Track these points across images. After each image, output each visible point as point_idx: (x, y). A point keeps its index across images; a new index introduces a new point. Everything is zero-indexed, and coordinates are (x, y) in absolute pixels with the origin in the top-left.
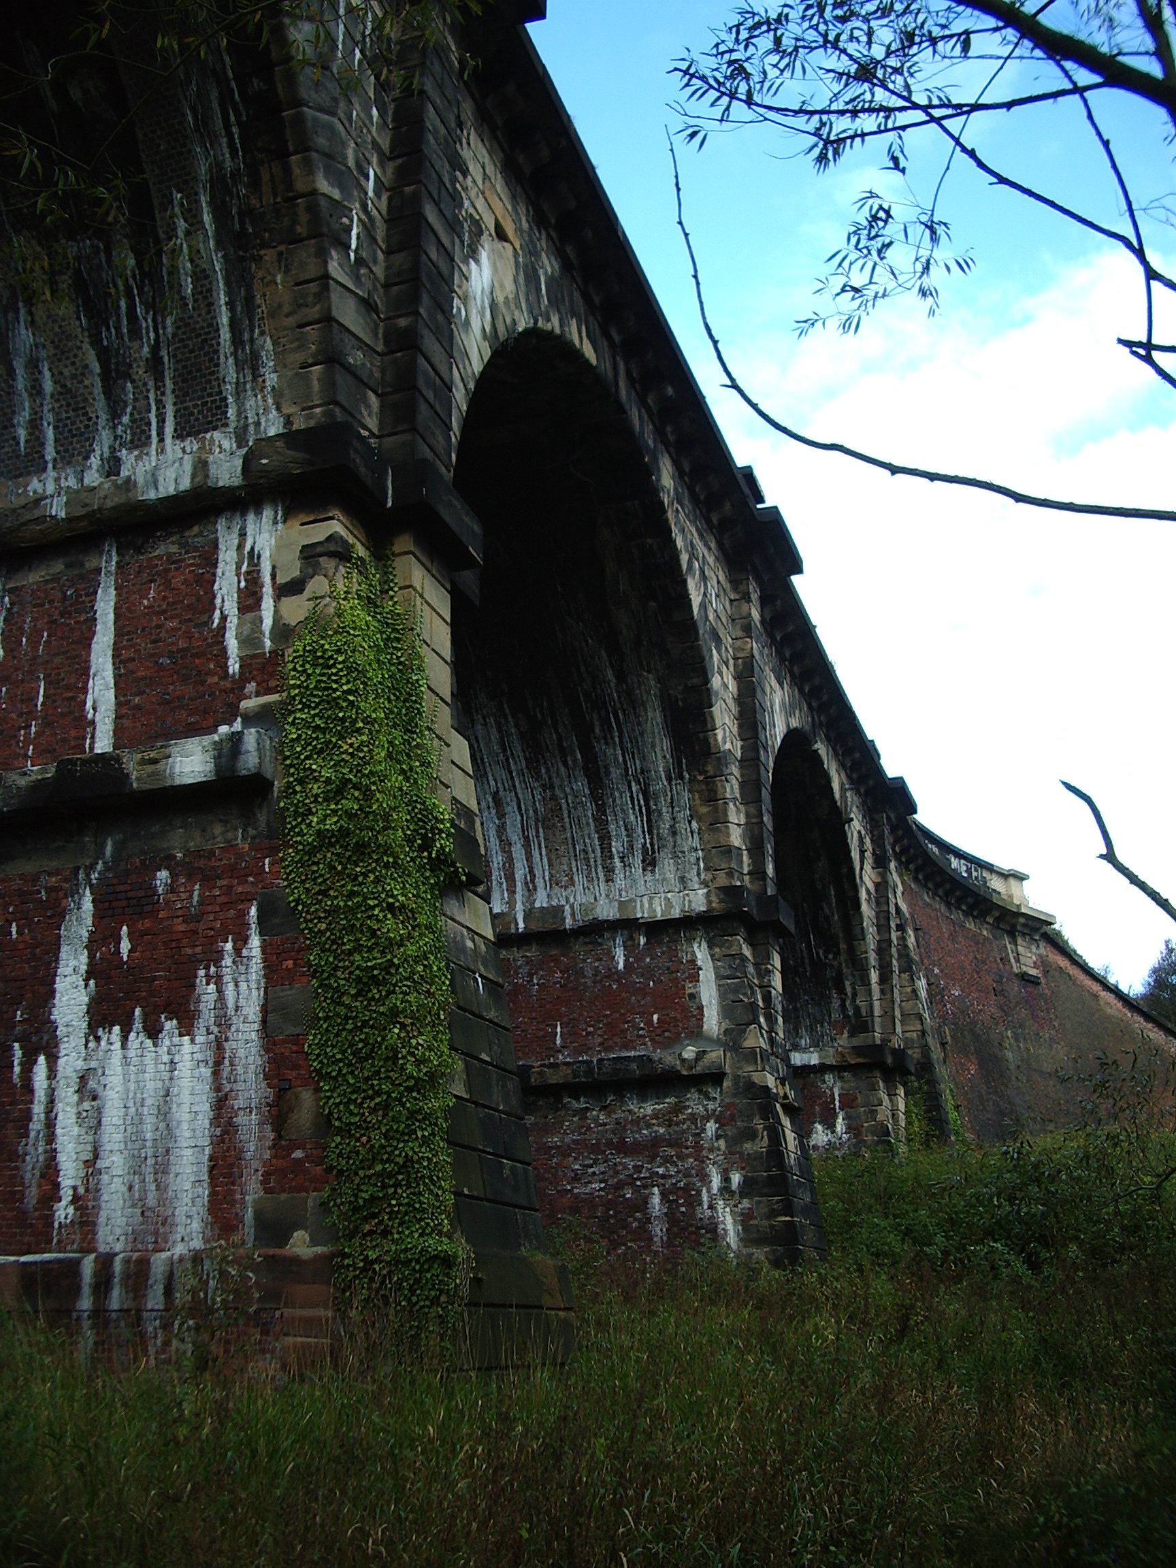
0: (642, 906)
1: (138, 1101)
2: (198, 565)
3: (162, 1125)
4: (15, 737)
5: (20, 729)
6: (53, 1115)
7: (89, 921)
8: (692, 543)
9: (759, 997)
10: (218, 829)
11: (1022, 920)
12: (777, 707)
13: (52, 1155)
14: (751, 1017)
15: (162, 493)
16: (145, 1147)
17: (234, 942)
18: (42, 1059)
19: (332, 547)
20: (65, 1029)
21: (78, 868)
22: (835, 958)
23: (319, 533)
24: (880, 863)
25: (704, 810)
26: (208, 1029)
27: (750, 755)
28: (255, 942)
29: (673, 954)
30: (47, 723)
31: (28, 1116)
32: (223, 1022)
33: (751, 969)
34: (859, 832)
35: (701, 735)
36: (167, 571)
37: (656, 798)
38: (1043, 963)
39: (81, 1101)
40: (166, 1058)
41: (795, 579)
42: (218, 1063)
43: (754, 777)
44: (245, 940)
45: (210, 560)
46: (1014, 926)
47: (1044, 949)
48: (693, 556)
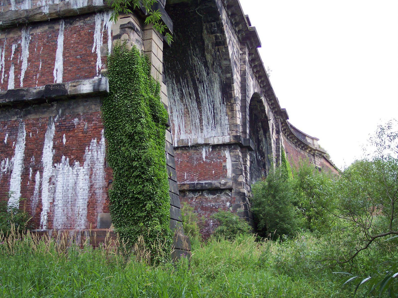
0: (211, 140)
1: (67, 185)
2: (89, 29)
3: (74, 192)
4: (32, 78)
5: (34, 75)
6: (41, 189)
7: (54, 133)
8: (230, 36)
9: (243, 167)
10: (93, 107)
11: (317, 152)
12: (251, 86)
13: (40, 201)
14: (241, 173)
15: (79, 7)
16: (68, 199)
17: (97, 140)
18: (38, 173)
19: (129, 25)
20: (45, 164)
21: (51, 117)
22: (263, 159)
23: (125, 21)
24: (278, 132)
25: (230, 113)
26: (88, 165)
27: (244, 98)
28: (103, 140)
29: (219, 154)
30: (42, 74)
31: (33, 189)
32: (93, 163)
33: (241, 159)
34: (272, 124)
35: (230, 92)
36: (79, 31)
37: (216, 110)
38: (322, 164)
39: (50, 185)
40: (75, 173)
41: (259, 49)
42: (91, 175)
43: (244, 105)
44: (100, 139)
45: (93, 27)
46: (314, 153)
47: (323, 160)
48: (230, 40)
